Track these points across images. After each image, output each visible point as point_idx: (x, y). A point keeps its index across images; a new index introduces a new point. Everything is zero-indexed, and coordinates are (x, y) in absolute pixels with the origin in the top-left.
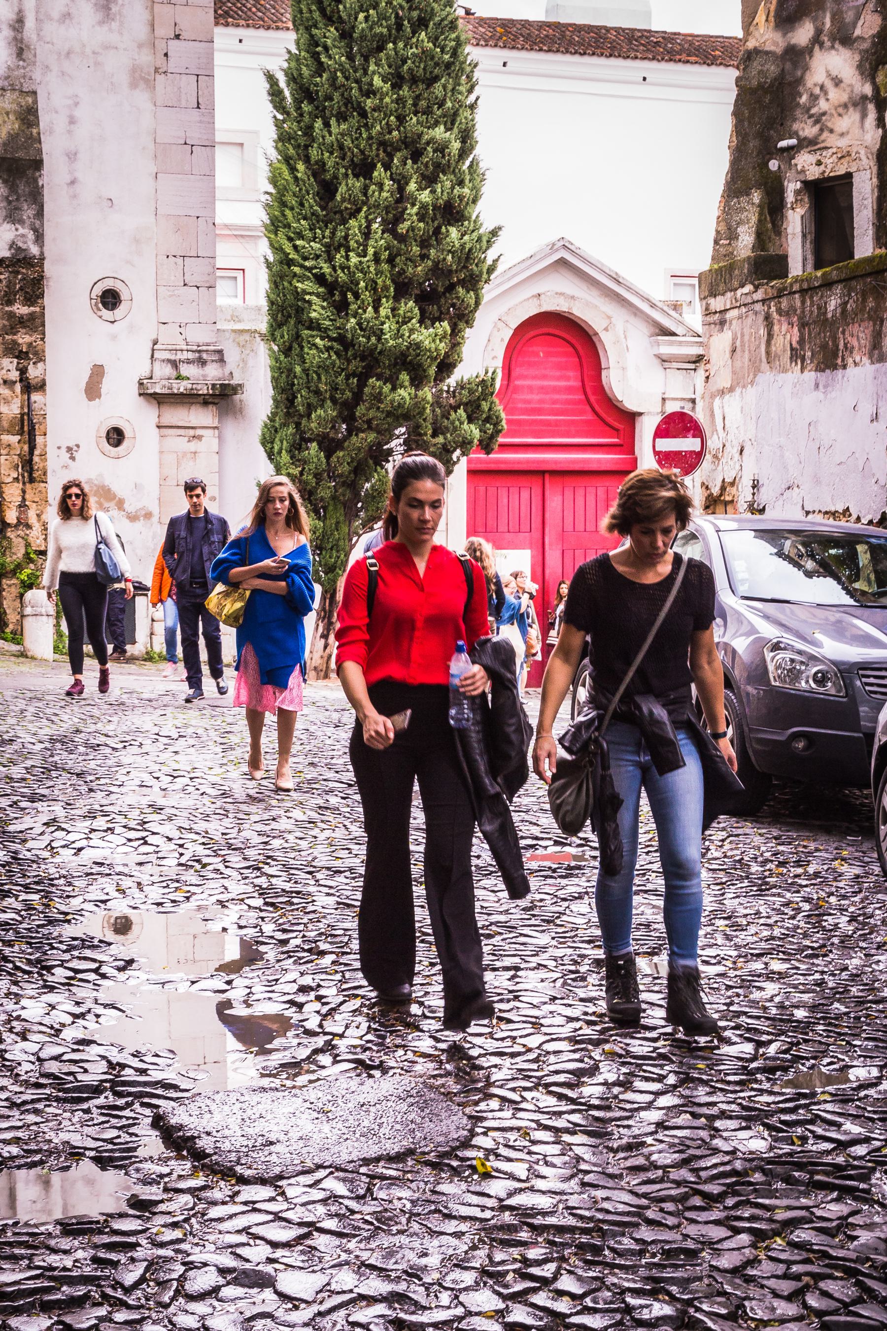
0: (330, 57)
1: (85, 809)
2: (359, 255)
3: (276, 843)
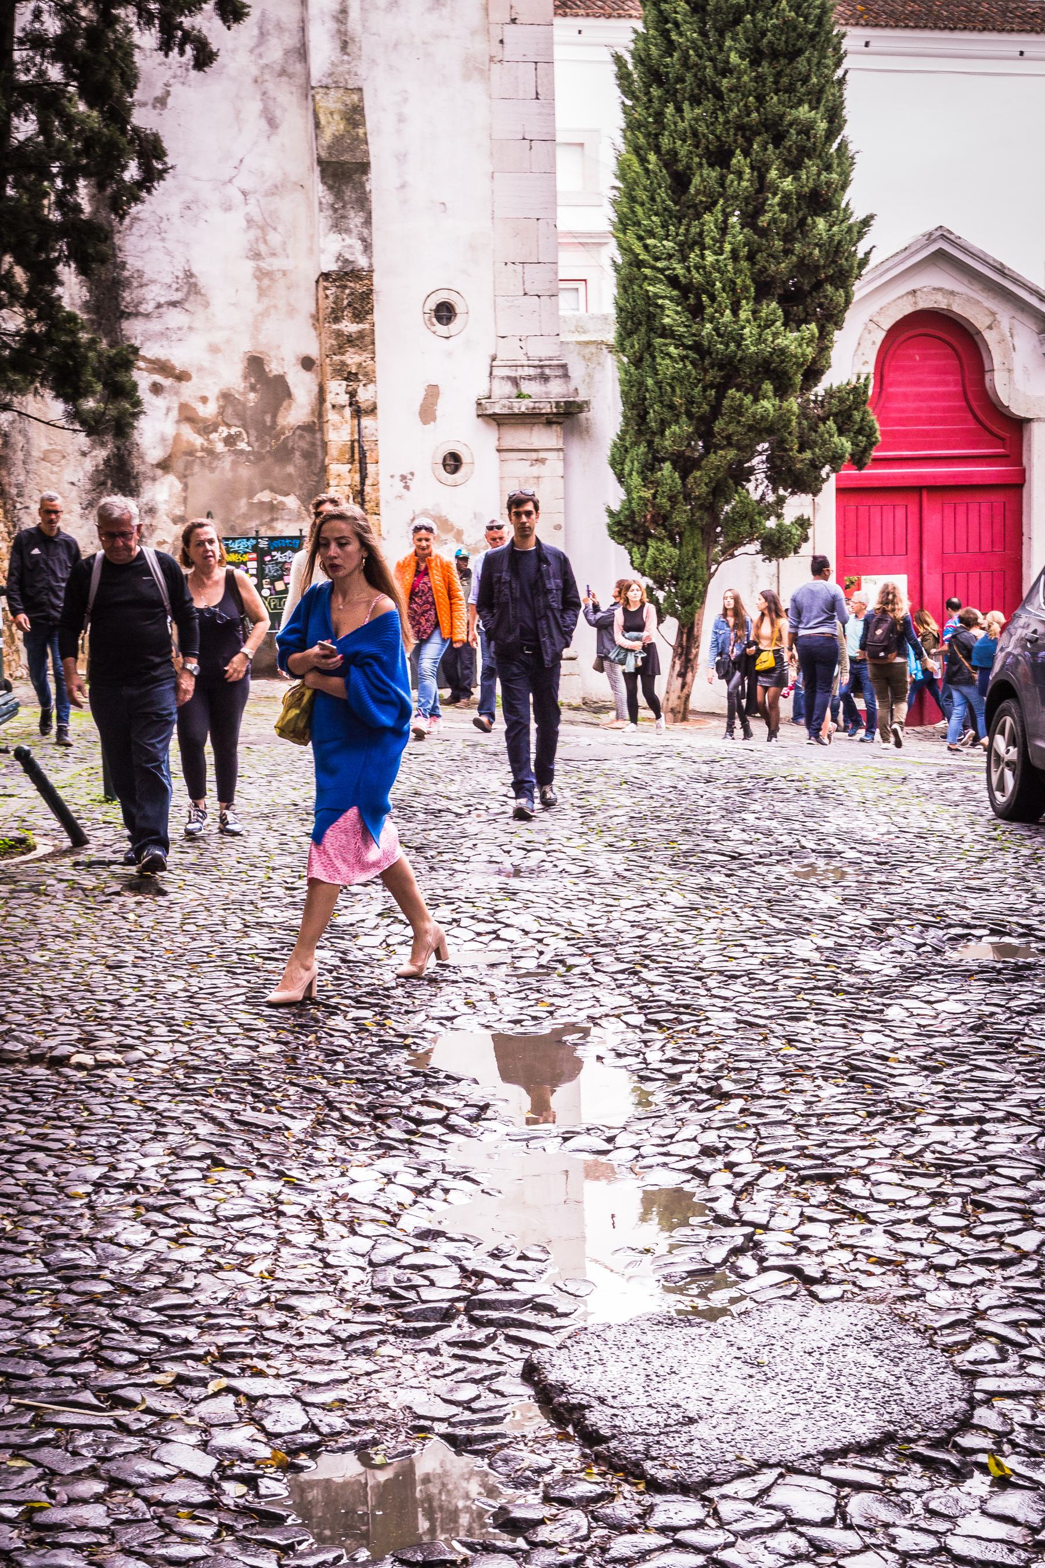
0: (681, 34)
2: (716, 253)
3: (654, 937)
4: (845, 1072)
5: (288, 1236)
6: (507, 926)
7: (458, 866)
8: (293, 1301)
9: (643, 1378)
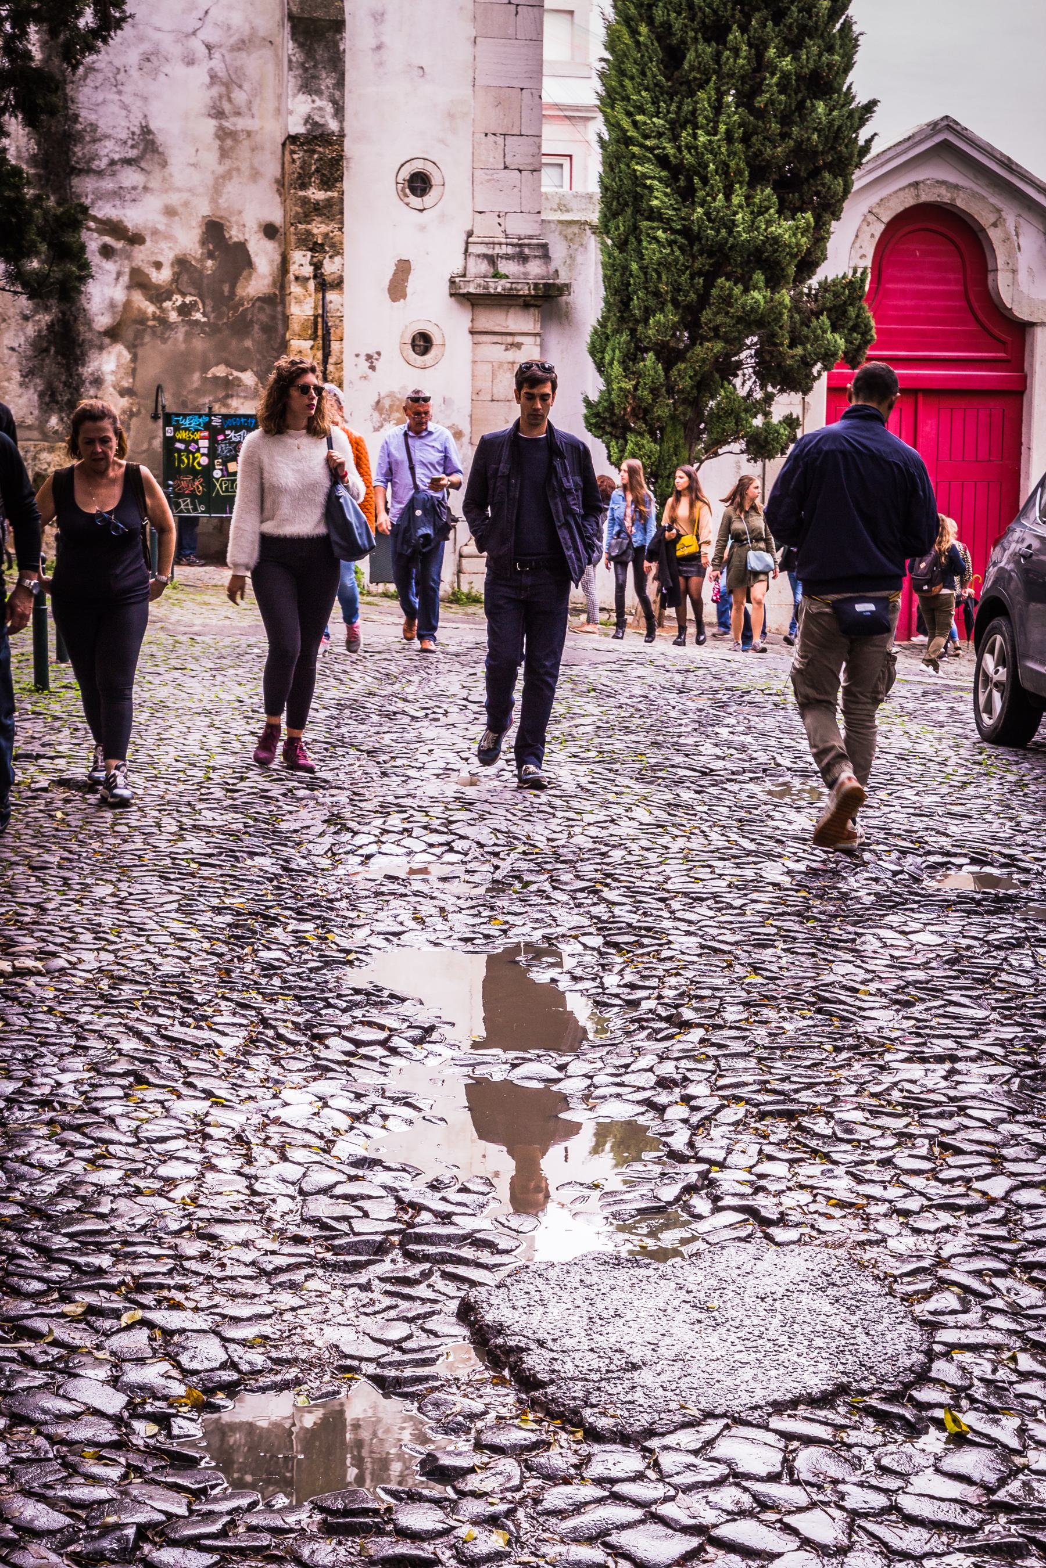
1: (376, 802)
2: (708, 133)
3: (617, 855)
4: (813, 1004)
5: (214, 1161)
8: (217, 1229)
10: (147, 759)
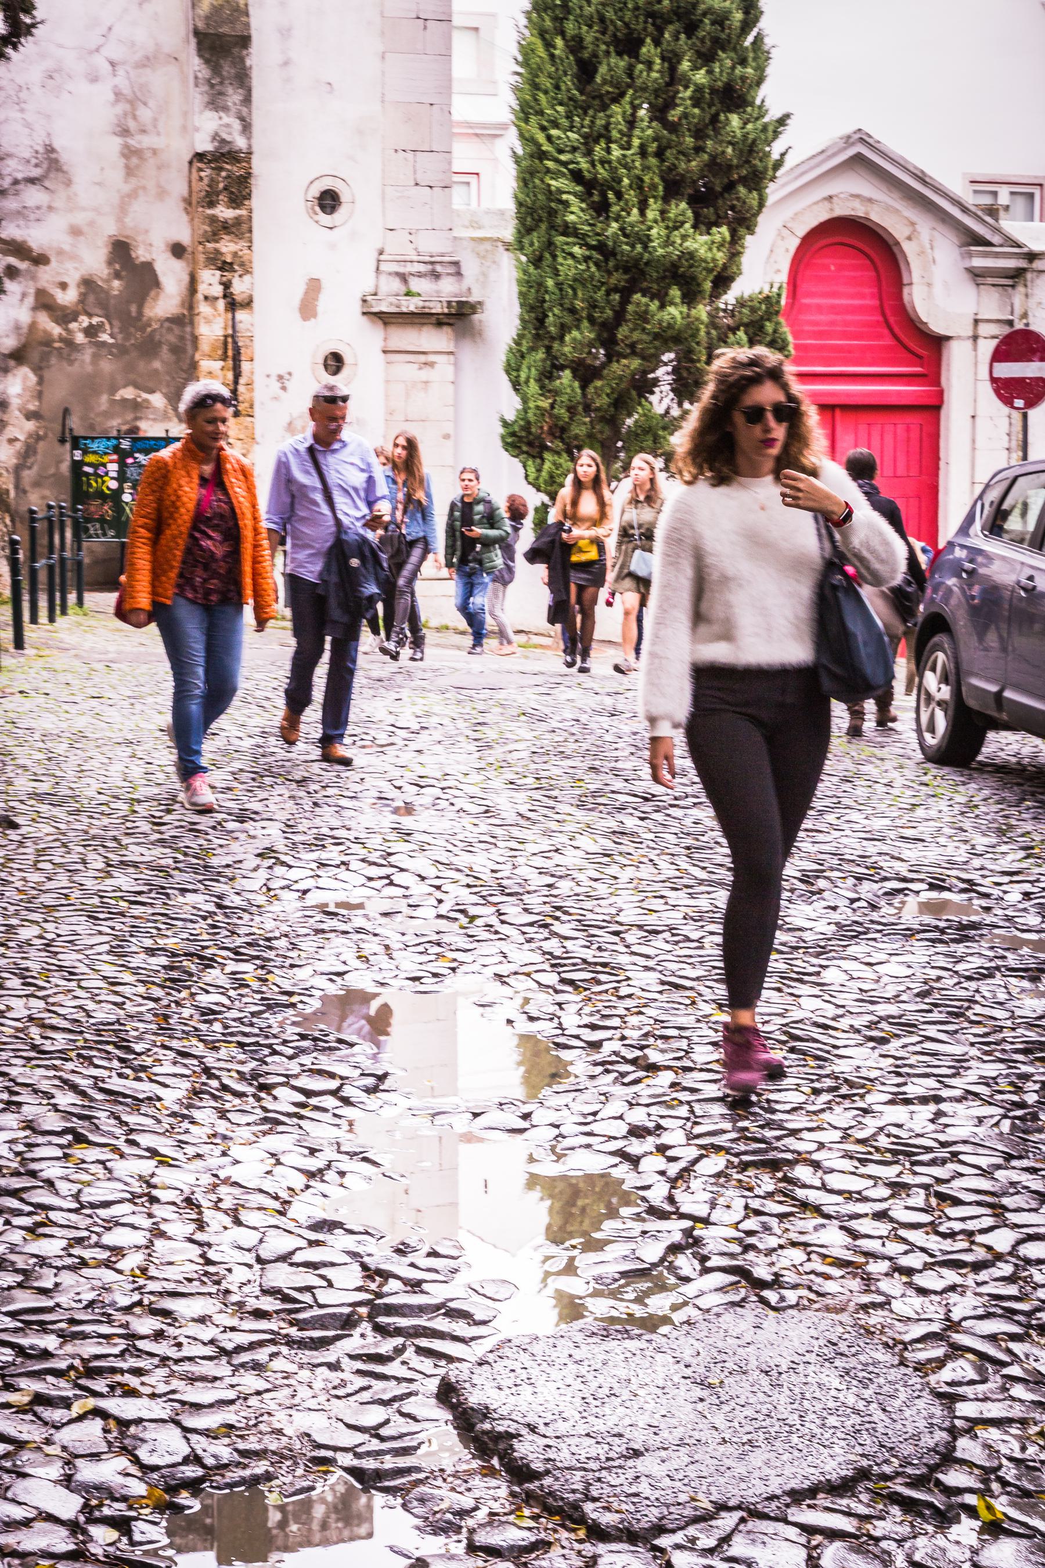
2: (622, 148)
3: (565, 887)
4: (784, 1043)
5: (163, 1227)
6: (402, 870)
7: (343, 802)
8: (168, 1304)
9: (578, 1401)
10: (69, 792)
